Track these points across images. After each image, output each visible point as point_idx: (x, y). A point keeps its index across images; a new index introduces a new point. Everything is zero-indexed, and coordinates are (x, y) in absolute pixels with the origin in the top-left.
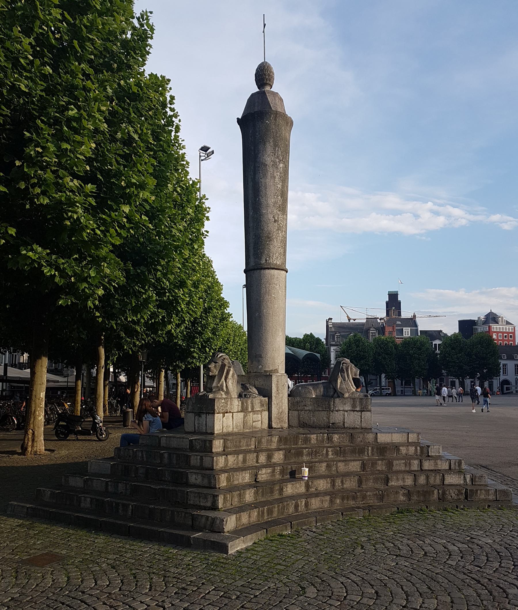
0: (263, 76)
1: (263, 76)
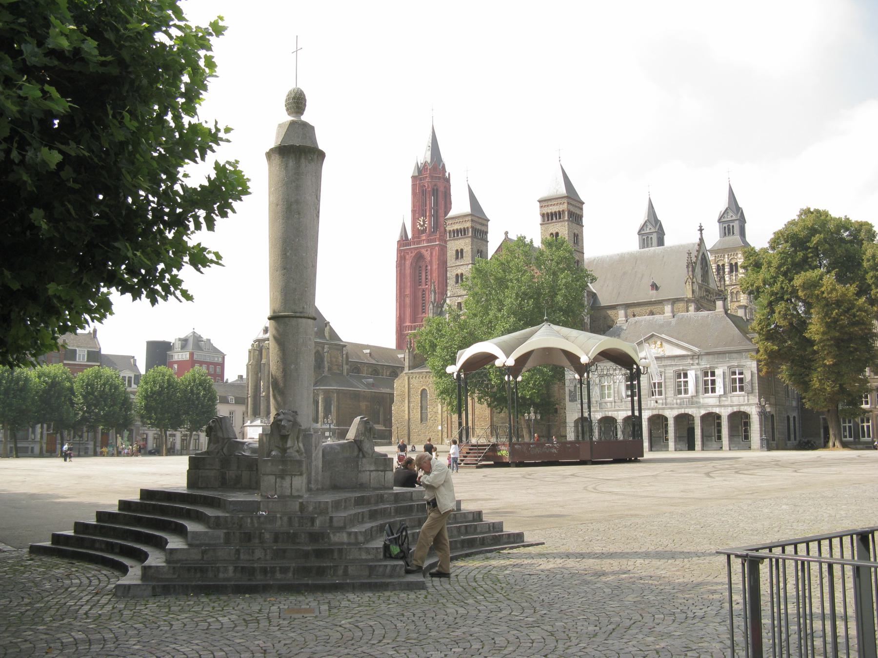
0: (297, 103)
1: (297, 103)
